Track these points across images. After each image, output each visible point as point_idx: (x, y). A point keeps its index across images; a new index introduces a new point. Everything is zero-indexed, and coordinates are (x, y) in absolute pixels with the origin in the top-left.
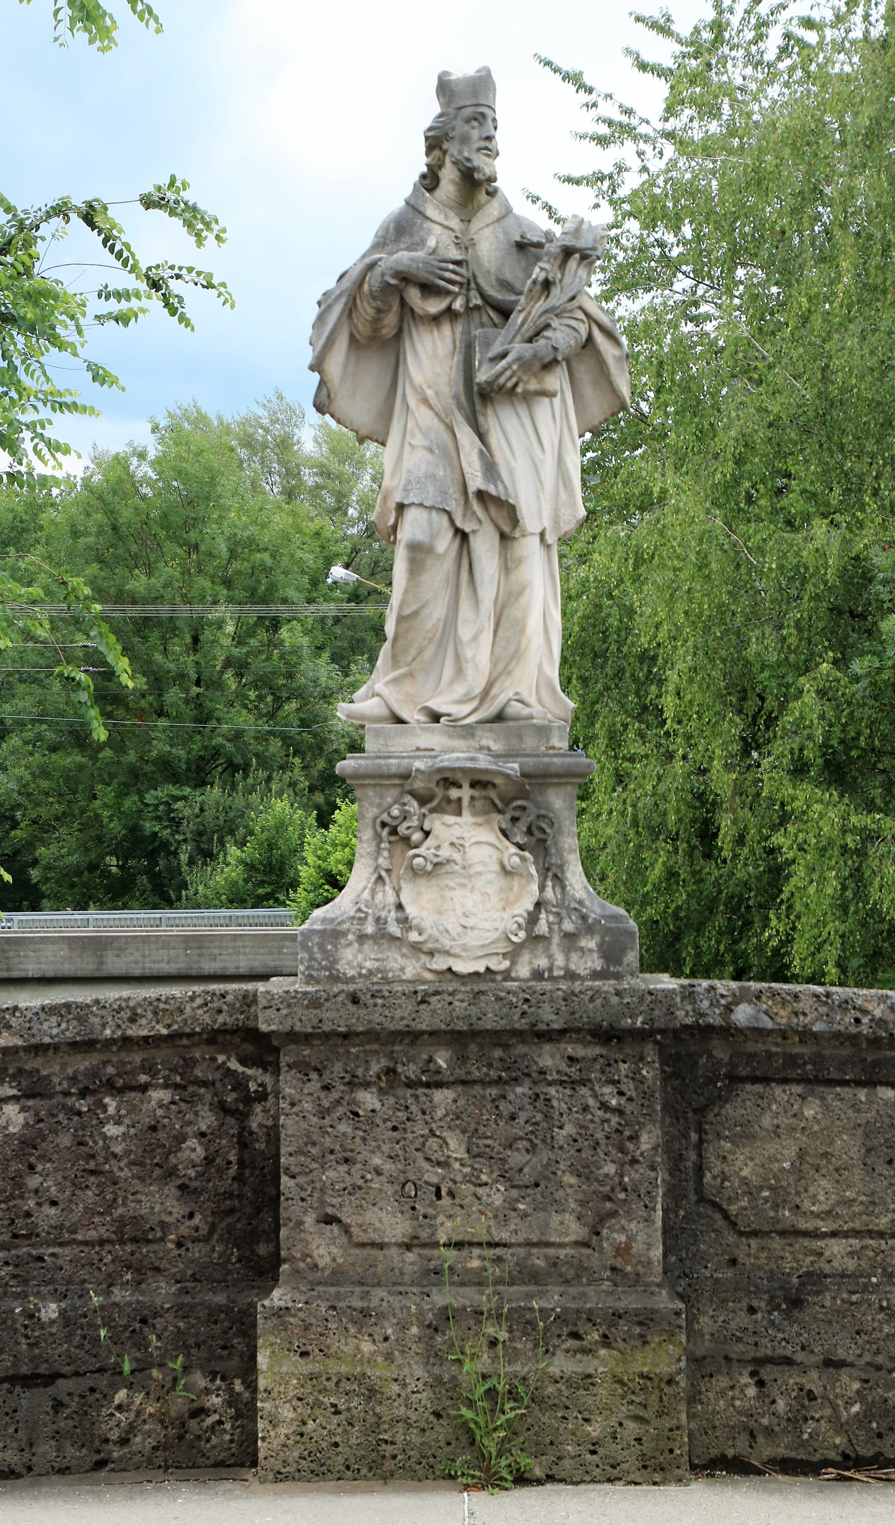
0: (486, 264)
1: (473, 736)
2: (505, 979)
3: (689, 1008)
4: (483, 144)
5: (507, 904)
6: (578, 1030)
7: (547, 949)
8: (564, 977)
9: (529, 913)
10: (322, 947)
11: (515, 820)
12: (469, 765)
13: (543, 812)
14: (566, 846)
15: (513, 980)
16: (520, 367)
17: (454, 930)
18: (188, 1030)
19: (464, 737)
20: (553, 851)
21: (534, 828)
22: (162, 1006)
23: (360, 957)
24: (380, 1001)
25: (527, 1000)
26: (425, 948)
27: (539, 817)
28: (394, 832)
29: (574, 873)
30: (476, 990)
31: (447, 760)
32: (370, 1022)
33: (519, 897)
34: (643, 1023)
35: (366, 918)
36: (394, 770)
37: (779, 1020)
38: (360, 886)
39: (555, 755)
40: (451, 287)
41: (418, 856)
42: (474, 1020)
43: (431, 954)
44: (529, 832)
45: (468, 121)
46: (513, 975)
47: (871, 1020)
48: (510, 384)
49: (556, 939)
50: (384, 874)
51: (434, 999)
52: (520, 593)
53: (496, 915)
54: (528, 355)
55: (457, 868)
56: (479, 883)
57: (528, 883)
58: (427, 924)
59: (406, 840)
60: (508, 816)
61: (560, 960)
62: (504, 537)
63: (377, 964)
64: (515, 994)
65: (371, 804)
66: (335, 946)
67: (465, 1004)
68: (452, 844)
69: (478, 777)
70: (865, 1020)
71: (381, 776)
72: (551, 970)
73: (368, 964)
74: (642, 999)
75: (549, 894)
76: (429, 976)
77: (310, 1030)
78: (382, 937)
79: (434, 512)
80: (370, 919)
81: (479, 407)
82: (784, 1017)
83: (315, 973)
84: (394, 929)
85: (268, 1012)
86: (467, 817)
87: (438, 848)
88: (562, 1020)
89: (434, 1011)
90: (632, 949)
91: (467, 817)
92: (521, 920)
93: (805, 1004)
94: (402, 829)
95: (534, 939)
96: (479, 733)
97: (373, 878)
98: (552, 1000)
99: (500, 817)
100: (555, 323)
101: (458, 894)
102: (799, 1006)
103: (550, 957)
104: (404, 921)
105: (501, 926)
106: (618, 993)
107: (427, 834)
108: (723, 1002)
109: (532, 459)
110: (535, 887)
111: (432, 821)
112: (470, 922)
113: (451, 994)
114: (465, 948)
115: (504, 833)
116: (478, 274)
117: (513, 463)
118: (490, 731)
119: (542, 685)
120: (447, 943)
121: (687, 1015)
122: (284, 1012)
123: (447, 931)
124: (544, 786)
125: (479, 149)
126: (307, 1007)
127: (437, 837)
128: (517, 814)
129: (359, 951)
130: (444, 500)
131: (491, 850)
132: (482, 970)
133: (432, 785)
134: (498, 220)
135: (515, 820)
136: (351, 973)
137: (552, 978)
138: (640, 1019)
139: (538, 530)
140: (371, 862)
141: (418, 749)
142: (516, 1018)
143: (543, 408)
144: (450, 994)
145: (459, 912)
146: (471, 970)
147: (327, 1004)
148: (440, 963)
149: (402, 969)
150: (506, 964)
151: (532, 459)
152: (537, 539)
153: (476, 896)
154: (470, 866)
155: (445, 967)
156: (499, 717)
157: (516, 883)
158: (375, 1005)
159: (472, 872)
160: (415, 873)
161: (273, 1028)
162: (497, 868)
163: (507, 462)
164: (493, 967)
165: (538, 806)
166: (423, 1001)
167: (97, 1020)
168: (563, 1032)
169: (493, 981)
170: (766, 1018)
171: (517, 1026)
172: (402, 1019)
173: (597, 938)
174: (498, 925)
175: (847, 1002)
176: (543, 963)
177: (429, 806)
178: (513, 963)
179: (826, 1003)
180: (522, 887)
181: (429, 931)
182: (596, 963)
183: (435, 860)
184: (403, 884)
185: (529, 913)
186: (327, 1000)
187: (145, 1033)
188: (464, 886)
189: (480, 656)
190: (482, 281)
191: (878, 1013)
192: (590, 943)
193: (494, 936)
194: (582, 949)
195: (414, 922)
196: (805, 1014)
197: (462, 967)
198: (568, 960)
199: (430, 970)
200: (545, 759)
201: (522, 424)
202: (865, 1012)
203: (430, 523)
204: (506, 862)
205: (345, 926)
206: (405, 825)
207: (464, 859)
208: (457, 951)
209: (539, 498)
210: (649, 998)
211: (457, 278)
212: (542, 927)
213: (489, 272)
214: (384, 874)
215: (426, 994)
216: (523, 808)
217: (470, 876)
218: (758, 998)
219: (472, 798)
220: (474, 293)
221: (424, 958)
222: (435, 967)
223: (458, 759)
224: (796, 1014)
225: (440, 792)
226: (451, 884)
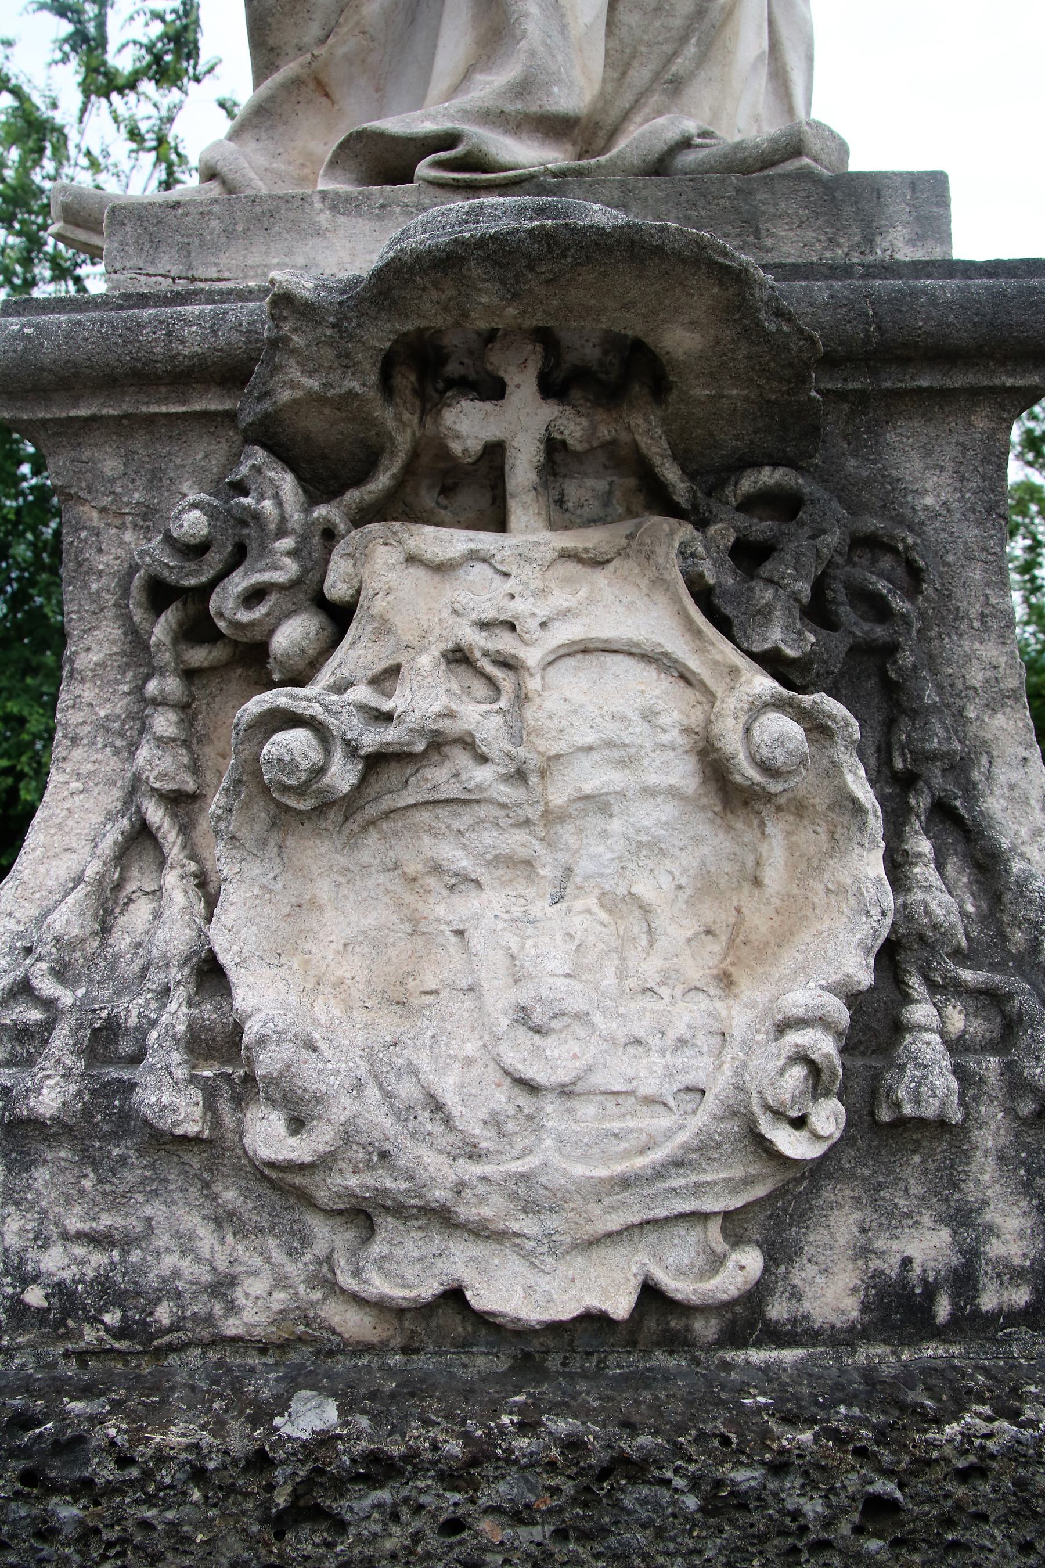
7: (947, 1180)
9: (854, 1000)
11: (749, 556)
13: (873, 524)
14: (977, 677)
15: (778, 1336)
17: (474, 1098)
20: (930, 695)
21: (838, 592)
24: (67, 1511)
25: (878, 1508)
26: (326, 1189)
28: (199, 628)
35: (48, 1026)
36: (193, 341)
38: (62, 869)
41: (290, 720)
43: (362, 1216)
46: (777, 1310)
49: (991, 1133)
50: (155, 814)
53: (688, 1014)
55: (483, 774)
56: (595, 850)
57: (836, 846)
58: (327, 1074)
59: (252, 661)
60: (723, 533)
65: (112, 513)
68: (459, 657)
72: (964, 1280)
73: (53, 1261)
80: (61, 1036)
84: (170, 1096)
86: (529, 532)
87: (387, 677)
91: (529, 532)
92: (824, 1046)
94: (226, 602)
95: (884, 1136)
101: (489, 907)
103: (962, 1218)
104: (218, 1043)
107: (339, 617)
110: (872, 865)
111: (360, 557)
112: (555, 1060)
113: (458, 1476)
114: (529, 1194)
120: (436, 1170)
123: (437, 1106)
124: (875, 408)
127: (384, 628)
128: (762, 528)
131: (652, 687)
132: (620, 1305)
133: (359, 384)
135: (749, 556)
137: (969, 1323)
140: (112, 764)
144: (453, 1477)
145: (499, 1003)
146: (566, 1310)
148: (405, 1269)
149: (222, 1286)
150: (749, 1262)
153: (584, 916)
155: (429, 1289)
157: (776, 847)
159: (558, 797)
160: (294, 810)
162: (682, 773)
164: (679, 1287)
166: (304, 1511)
174: (699, 1068)
177: (352, 496)
178: (779, 1253)
180: (806, 868)
183: (372, 739)
184: (224, 864)
185: (854, 1000)
193: (683, 1128)
195: (266, 1063)
197: (516, 1291)
199: (381, 1306)
204: (732, 743)
206: (239, 582)
208: (490, 1209)
212: (928, 1075)
214: (155, 814)
216: (785, 505)
217: (552, 817)
219: (554, 449)
221: (327, 1236)
225: (400, 427)
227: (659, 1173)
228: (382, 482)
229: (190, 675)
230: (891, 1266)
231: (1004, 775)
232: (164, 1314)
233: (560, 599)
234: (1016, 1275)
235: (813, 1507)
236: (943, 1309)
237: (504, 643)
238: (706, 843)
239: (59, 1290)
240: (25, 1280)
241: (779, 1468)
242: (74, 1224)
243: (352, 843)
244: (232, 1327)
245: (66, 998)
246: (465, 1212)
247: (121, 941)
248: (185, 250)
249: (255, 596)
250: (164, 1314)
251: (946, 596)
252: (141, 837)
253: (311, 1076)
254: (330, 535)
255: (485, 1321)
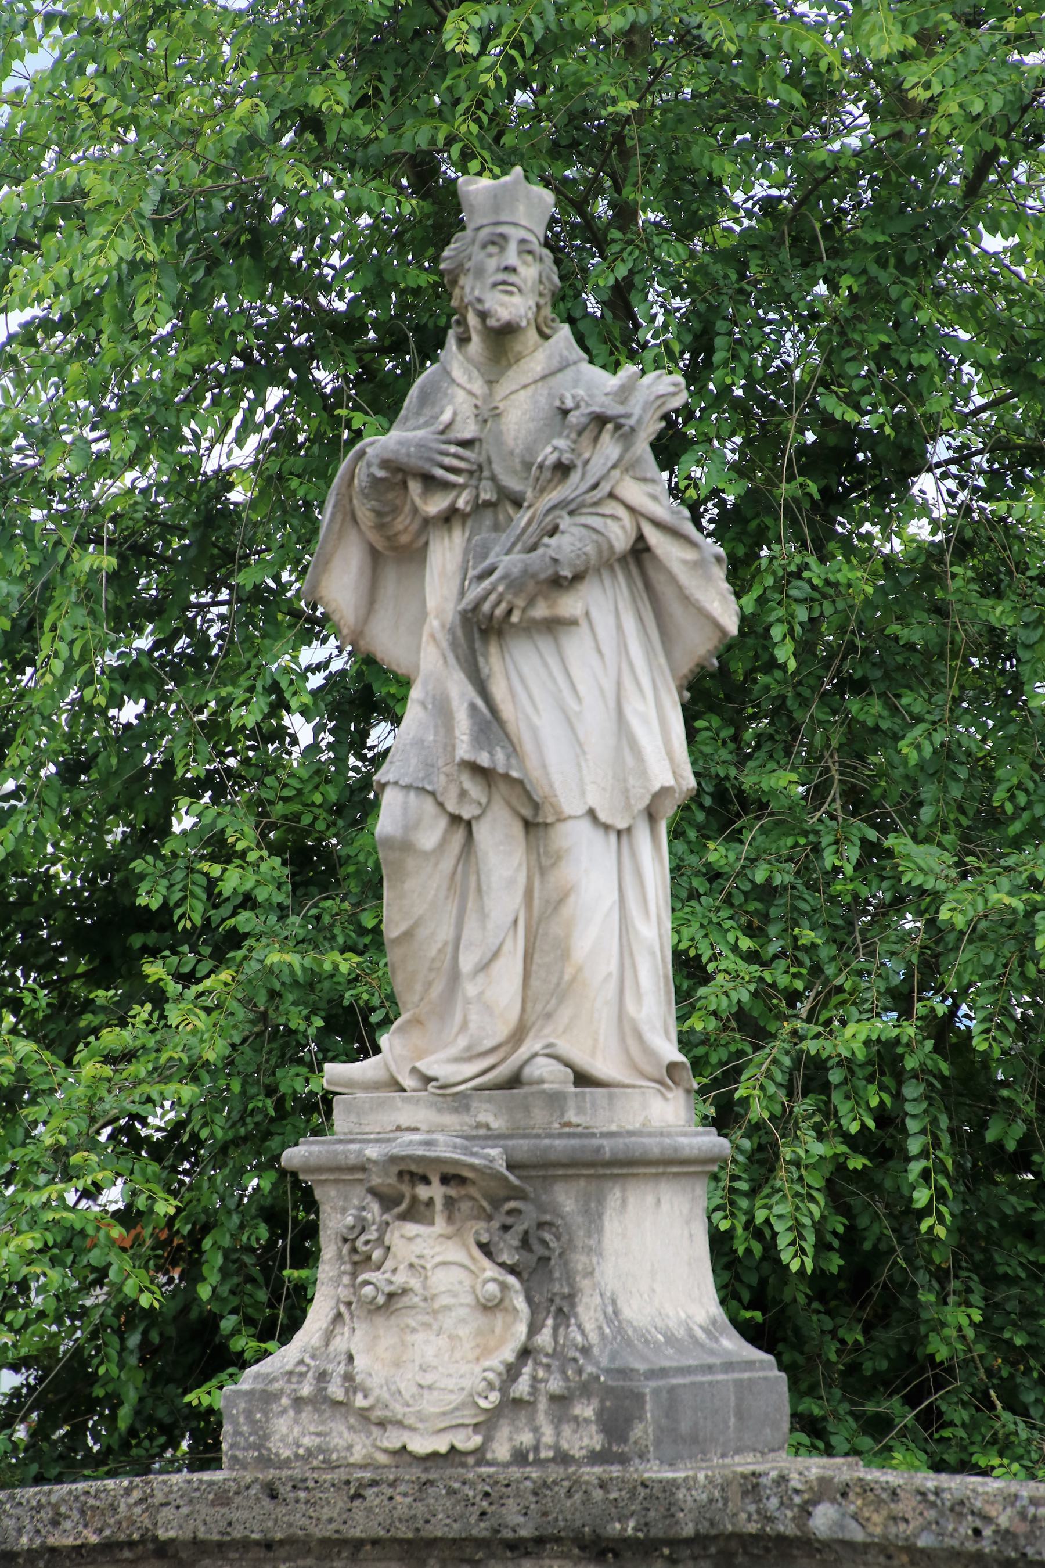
0: (511, 443)
1: (467, 1108)
2: (479, 1463)
3: (752, 1508)
4: (501, 276)
5: (486, 1351)
6: (558, 1540)
7: (532, 1419)
8: (553, 1460)
10: (249, 1414)
12: (420, 1152)
13: (548, 1218)
14: (580, 1267)
15: (489, 1464)
16: (508, 587)
17: (408, 1389)
18: (122, 1537)
19: (456, 1110)
22: (91, 1501)
23: (297, 1430)
24: (302, 1495)
25: (487, 1494)
27: (541, 1225)
28: (354, 1250)
29: (588, 1308)
30: (424, 1477)
31: (408, 1144)
32: (290, 1525)
33: (502, 1342)
34: (636, 1529)
37: (871, 1528)
38: (317, 1326)
39: (570, 1135)
40: (452, 478)
42: (420, 1524)
44: (525, 1243)
45: (484, 246)
46: (489, 1456)
47: (996, 1532)
48: (499, 612)
49: (543, 1404)
50: (343, 1309)
51: (369, 1492)
52: (561, 901)
53: (464, 1368)
54: (516, 571)
55: (416, 1299)
56: (448, 1321)
58: (374, 1383)
60: (496, 1224)
61: (548, 1436)
62: (528, 825)
63: (318, 1440)
64: (472, 1485)
66: (266, 1414)
67: (410, 1499)
68: (411, 1266)
69: (451, 1170)
70: (987, 1532)
71: (339, 1169)
72: (536, 1449)
73: (307, 1441)
74: (633, 1492)
75: (544, 1338)
76: (382, 1458)
77: (216, 1537)
78: (321, 1401)
79: (412, 794)
80: (310, 1375)
81: (478, 645)
82: (877, 1524)
83: (240, 1454)
85: (165, 1511)
87: (394, 1271)
88: (531, 1524)
89: (369, 1510)
90: (641, 1419)
92: (491, 1376)
93: (907, 1505)
96: (475, 1104)
97: (331, 1315)
98: (518, 1495)
99: (482, 1225)
100: (565, 522)
101: (419, 1337)
102: (897, 1508)
103: (536, 1430)
105: (467, 1383)
106: (602, 1485)
108: (797, 1500)
109: (564, 711)
112: (428, 1379)
113: (392, 1484)
114: (421, 1417)
115: (486, 1249)
116: (494, 458)
117: (535, 719)
118: (489, 1100)
119: (627, 1029)
120: (398, 1410)
121: (749, 1519)
122: (185, 1510)
124: (548, 1181)
125: (495, 285)
126: (213, 1504)
128: (509, 1221)
129: (296, 1421)
130: (428, 776)
133: (392, 1180)
134: (544, 378)
136: (286, 1453)
137: (539, 1462)
138: (631, 1524)
139: (581, 810)
141: (399, 1129)
142: (473, 1520)
143: (577, 647)
146: (429, 1450)
147: (238, 1500)
148: (393, 1439)
149: (349, 1448)
150: (477, 1440)
151: (564, 711)
152: (584, 826)
153: (443, 1341)
154: (433, 1297)
156: (515, 1081)
157: (499, 1320)
158: (297, 1501)
161: (172, 1534)
162: (469, 1299)
163: (528, 718)
164: (460, 1446)
165: (542, 1208)
166: (358, 1496)
167: (10, 1523)
168: (540, 1541)
169: (464, 1465)
170: (853, 1524)
171: (475, 1532)
172: (331, 1520)
173: (595, 1403)
175: (962, 1503)
176: (526, 1438)
177: (397, 1211)
178: (488, 1439)
179: (933, 1505)
181: (376, 1392)
182: (592, 1439)
183: (388, 1289)
186: (237, 1493)
187: (69, 1541)
188: (427, 1326)
189: (501, 991)
190: (497, 468)
191: (1003, 1521)
192: (586, 1410)
193: (457, 1399)
194: (576, 1419)
196: (906, 1521)
197: (420, 1445)
198: (558, 1434)
199: (385, 1451)
200: (547, 1142)
201: (546, 665)
202: (987, 1519)
203: (405, 808)
205: (277, 1386)
206: (363, 1238)
207: (425, 1287)
208: (410, 1421)
209: (579, 765)
210: (642, 1492)
211: (462, 465)
213: (512, 453)
215: (362, 1485)
217: (435, 1313)
218: (844, 1495)
220: (486, 484)
221: (376, 1431)
222: (386, 1444)
223: (410, 1143)
224: (894, 1519)
225: (405, 1188)
226: (412, 1323)
227: (453, 1411)
228: (403, 1206)
229: (355, 1264)
230: (517, 1444)
231: (585, 1299)
232: (334, 1456)
233: (437, 1249)
234: (550, 1447)
235: (471, 1493)
236: (531, 1457)
237: (422, 1262)
238: (480, 1320)
239: (308, 1450)
240: (299, 1446)
241: (464, 1483)
242: (312, 1429)
243: (388, 1318)
244: (352, 1460)
245: (312, 1363)
246: (406, 1422)
247: (331, 1348)
248: (358, 1114)
249: (367, 1242)
250: (334, 1456)
251: (571, 1240)
252: (339, 1316)
253: (369, 1383)
254: (388, 1224)
255: (410, 1453)
